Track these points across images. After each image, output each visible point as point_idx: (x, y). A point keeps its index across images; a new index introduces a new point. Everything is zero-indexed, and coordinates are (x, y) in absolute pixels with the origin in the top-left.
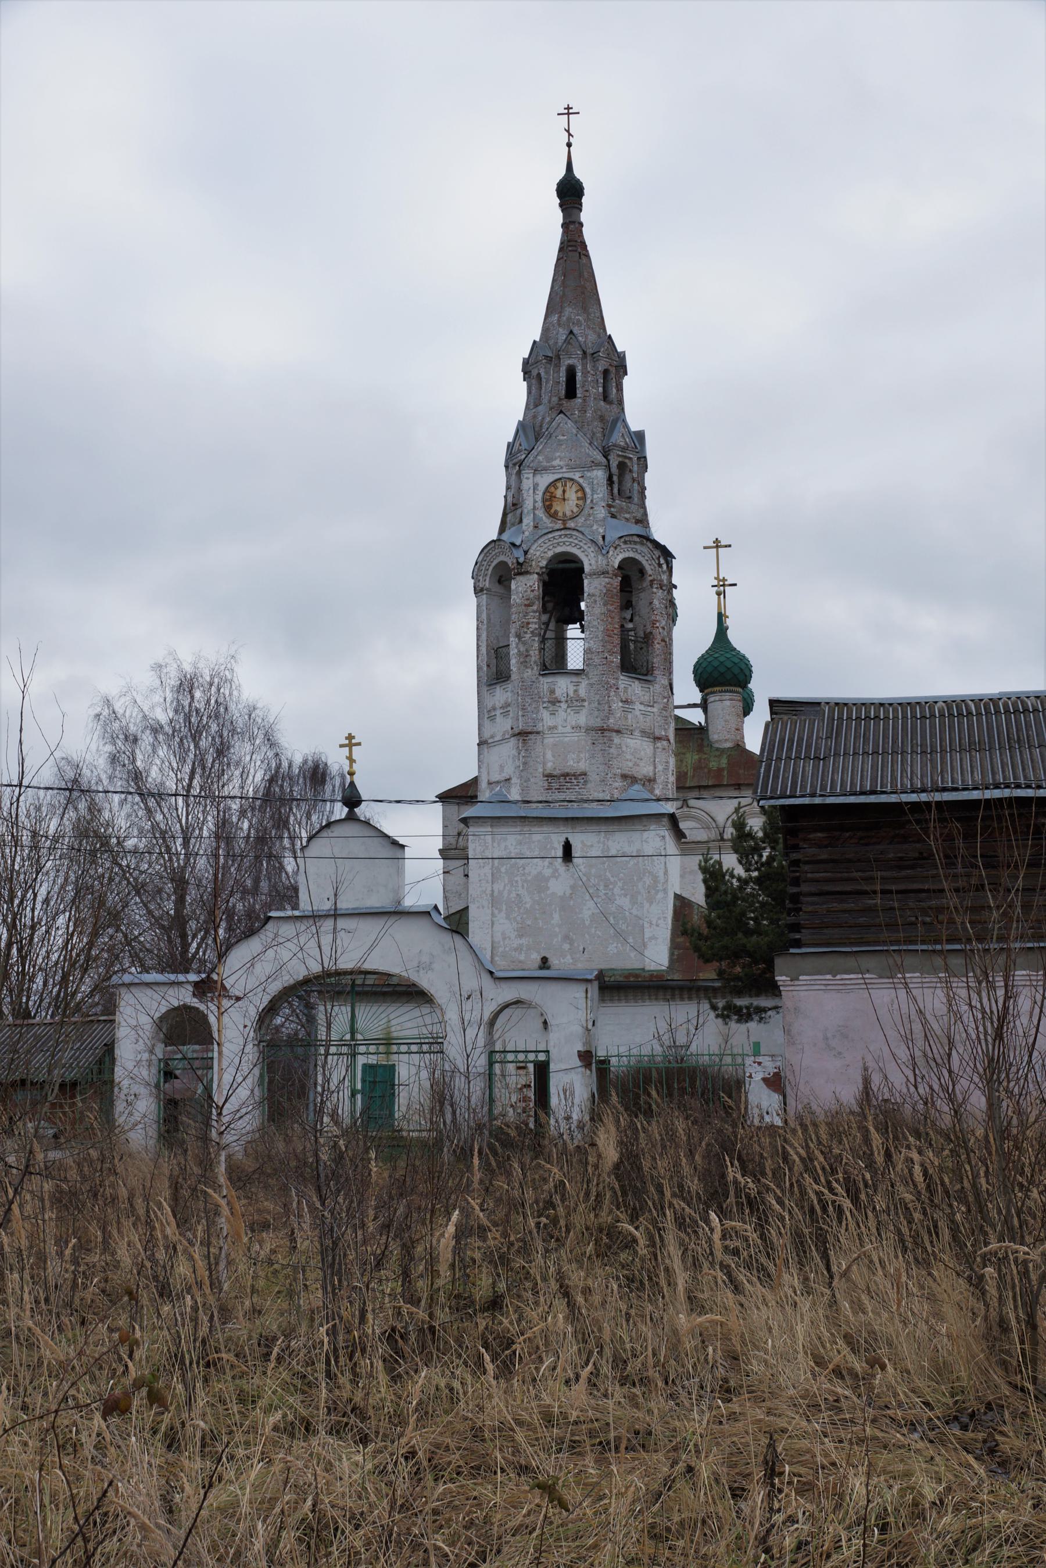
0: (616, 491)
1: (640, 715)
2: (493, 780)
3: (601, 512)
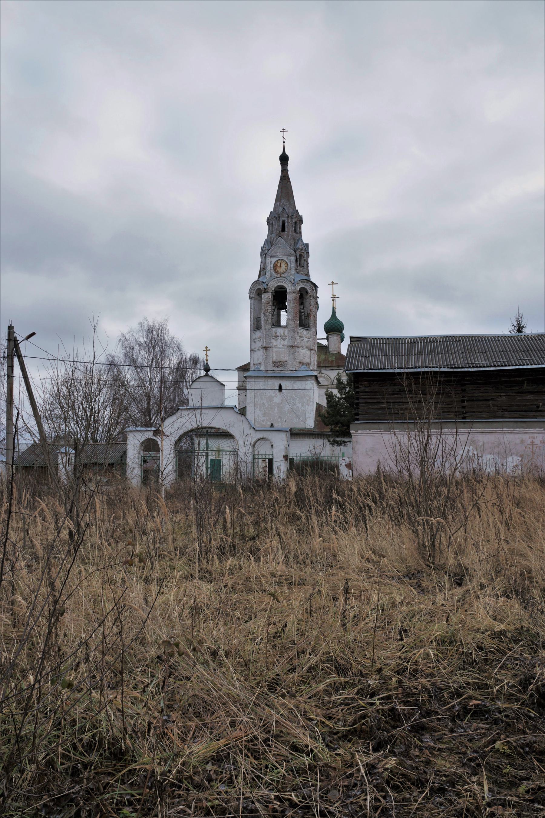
1: (306, 341)
3: (293, 271)
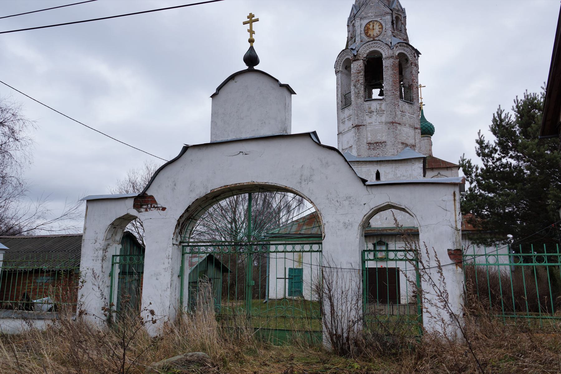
0: (395, 27)
1: (407, 119)
2: (344, 148)
3: (389, 33)
